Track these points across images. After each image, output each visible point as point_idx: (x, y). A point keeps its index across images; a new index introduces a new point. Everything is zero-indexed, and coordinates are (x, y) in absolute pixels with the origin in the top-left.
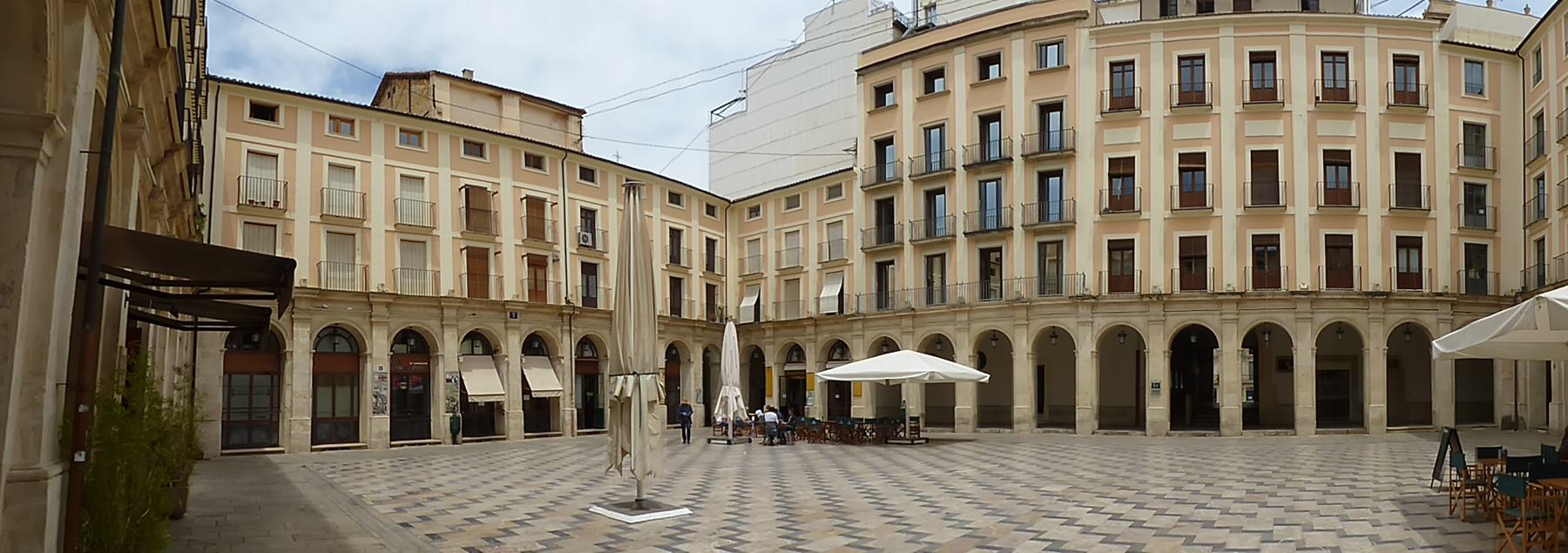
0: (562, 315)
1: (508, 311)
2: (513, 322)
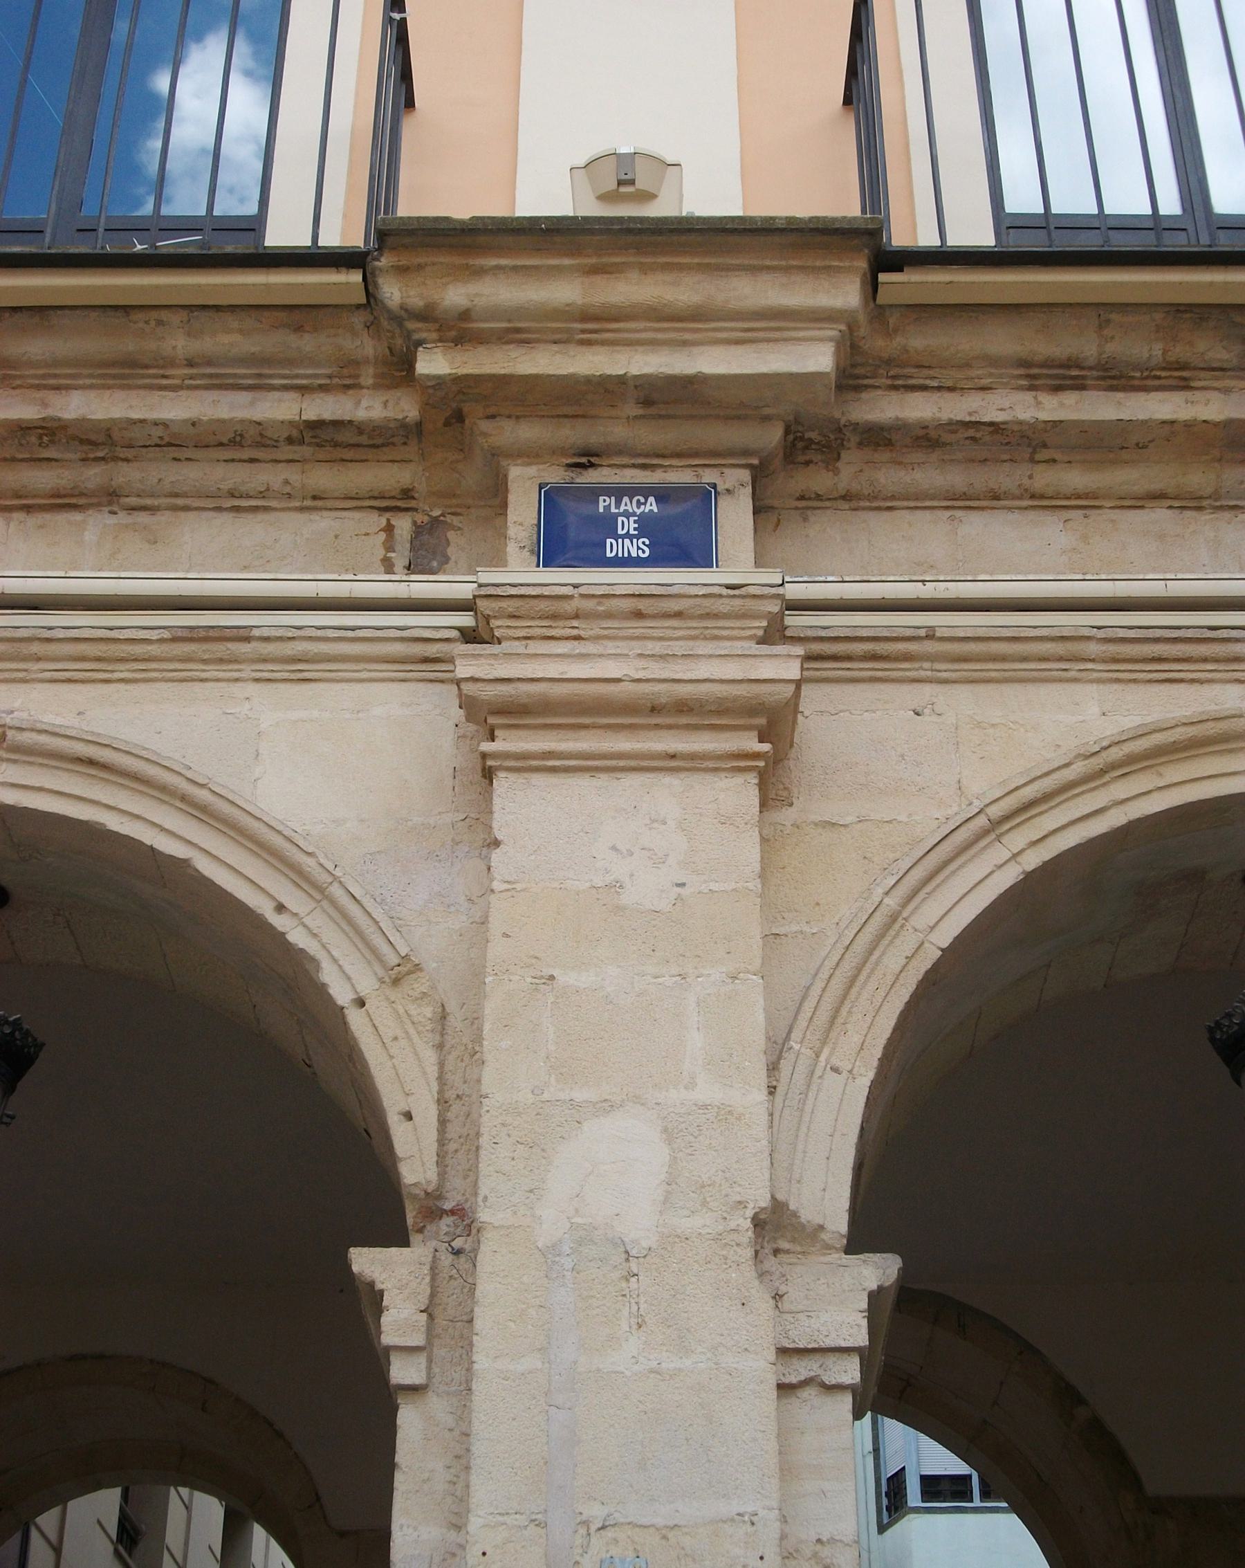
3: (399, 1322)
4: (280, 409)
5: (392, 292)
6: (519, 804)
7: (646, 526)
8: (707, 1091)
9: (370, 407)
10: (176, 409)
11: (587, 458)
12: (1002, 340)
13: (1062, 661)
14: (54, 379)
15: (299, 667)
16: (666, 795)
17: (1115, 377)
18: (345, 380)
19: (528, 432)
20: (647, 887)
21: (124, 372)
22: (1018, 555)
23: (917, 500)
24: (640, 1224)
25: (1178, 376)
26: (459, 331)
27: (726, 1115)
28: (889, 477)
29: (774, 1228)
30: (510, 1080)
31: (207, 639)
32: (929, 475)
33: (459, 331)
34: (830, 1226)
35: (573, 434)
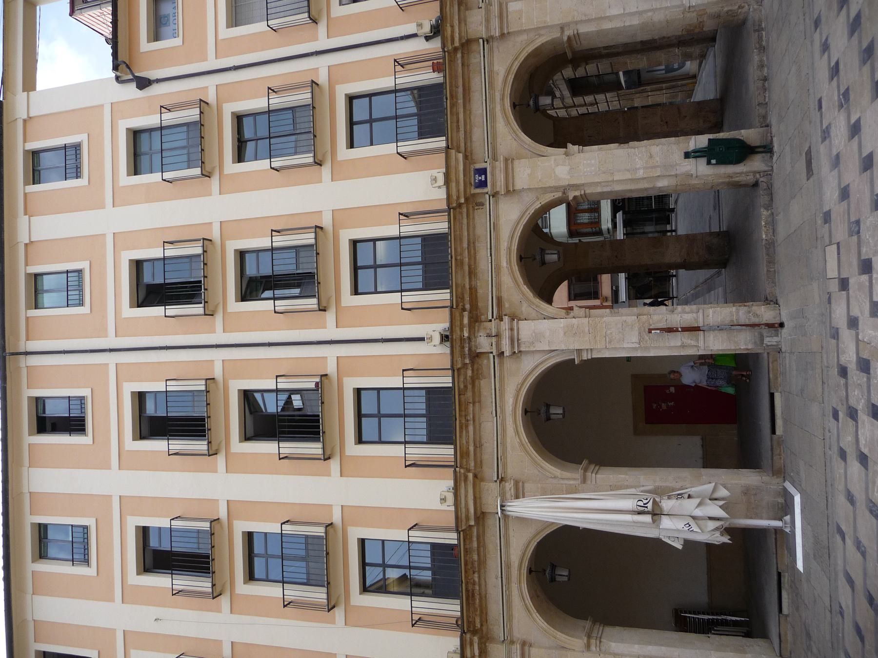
0: (467, 44)
1: (470, 188)
2: (497, 179)
3: (577, 193)
4: (465, 221)
5: (454, 205)
6: (519, 186)
7: (480, 176)
8: (552, 162)
9: (465, 210)
10: (465, 234)
11: (471, 184)
12: (455, 134)
13: (494, 128)
14: (462, 248)
15: (497, 217)
16: (517, 170)
17: (458, 122)
18: (461, 213)
19: (468, 190)
20: (529, 171)
21: (461, 240)
22: (478, 134)
23: (471, 146)
24: (567, 168)
25: (458, 114)
26: (458, 197)
27: (555, 160)
28: (469, 149)
29: (567, 154)
30: (552, 183)
31: (495, 227)
32: (469, 144)
33: (458, 197)
34: (516, 503)
35: (468, 185)
